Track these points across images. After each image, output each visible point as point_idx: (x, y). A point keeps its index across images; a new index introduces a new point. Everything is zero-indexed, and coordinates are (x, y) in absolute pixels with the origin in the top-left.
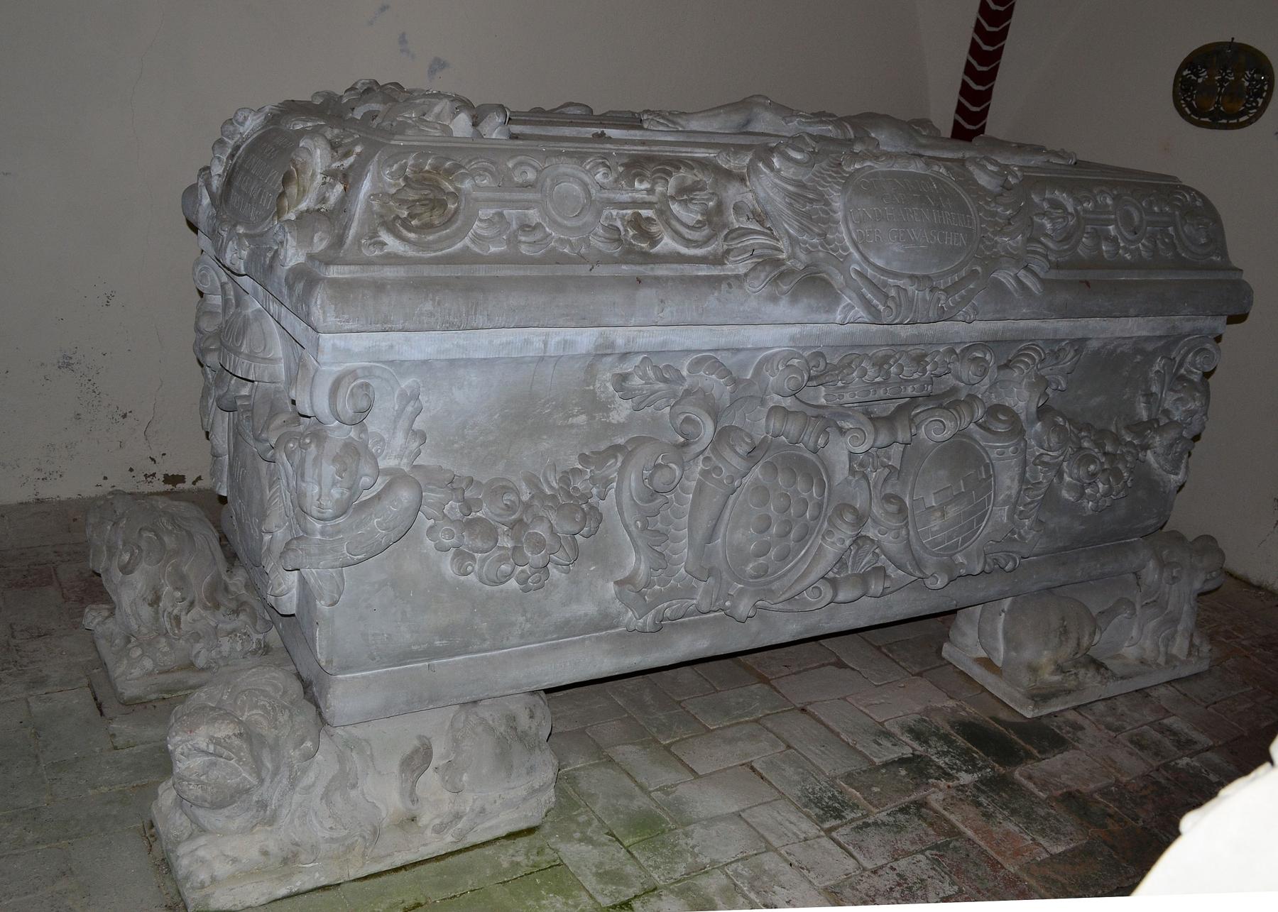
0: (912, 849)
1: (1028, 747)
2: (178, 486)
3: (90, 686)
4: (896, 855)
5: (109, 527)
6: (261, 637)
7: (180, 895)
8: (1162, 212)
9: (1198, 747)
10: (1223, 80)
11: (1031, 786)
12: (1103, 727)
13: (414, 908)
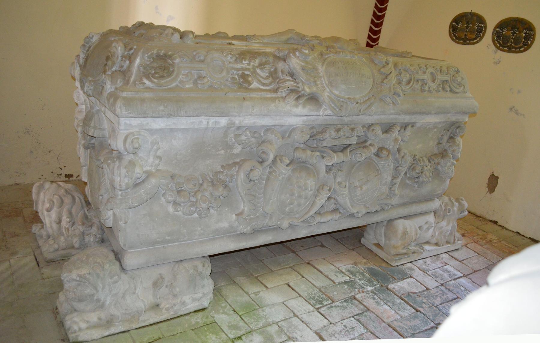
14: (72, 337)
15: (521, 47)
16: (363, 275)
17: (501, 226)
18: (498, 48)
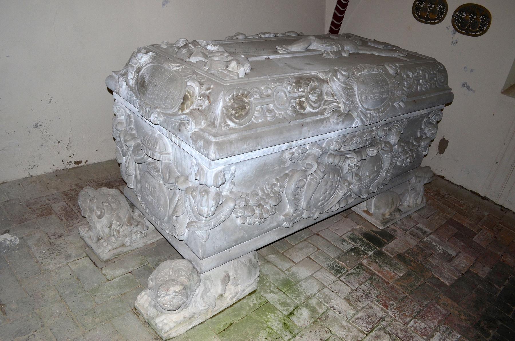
0: (364, 281)
1: (384, 239)
2: (80, 164)
3: (87, 256)
4: (360, 283)
5: (88, 201)
6: (145, 232)
7: (157, 334)
8: (434, 73)
9: (428, 233)
10: (430, 7)
11: (388, 253)
12: (401, 230)
13: (231, 325)
14: (164, 336)
15: (477, 32)
16: (363, 241)
17: (447, 180)
18: (456, 30)
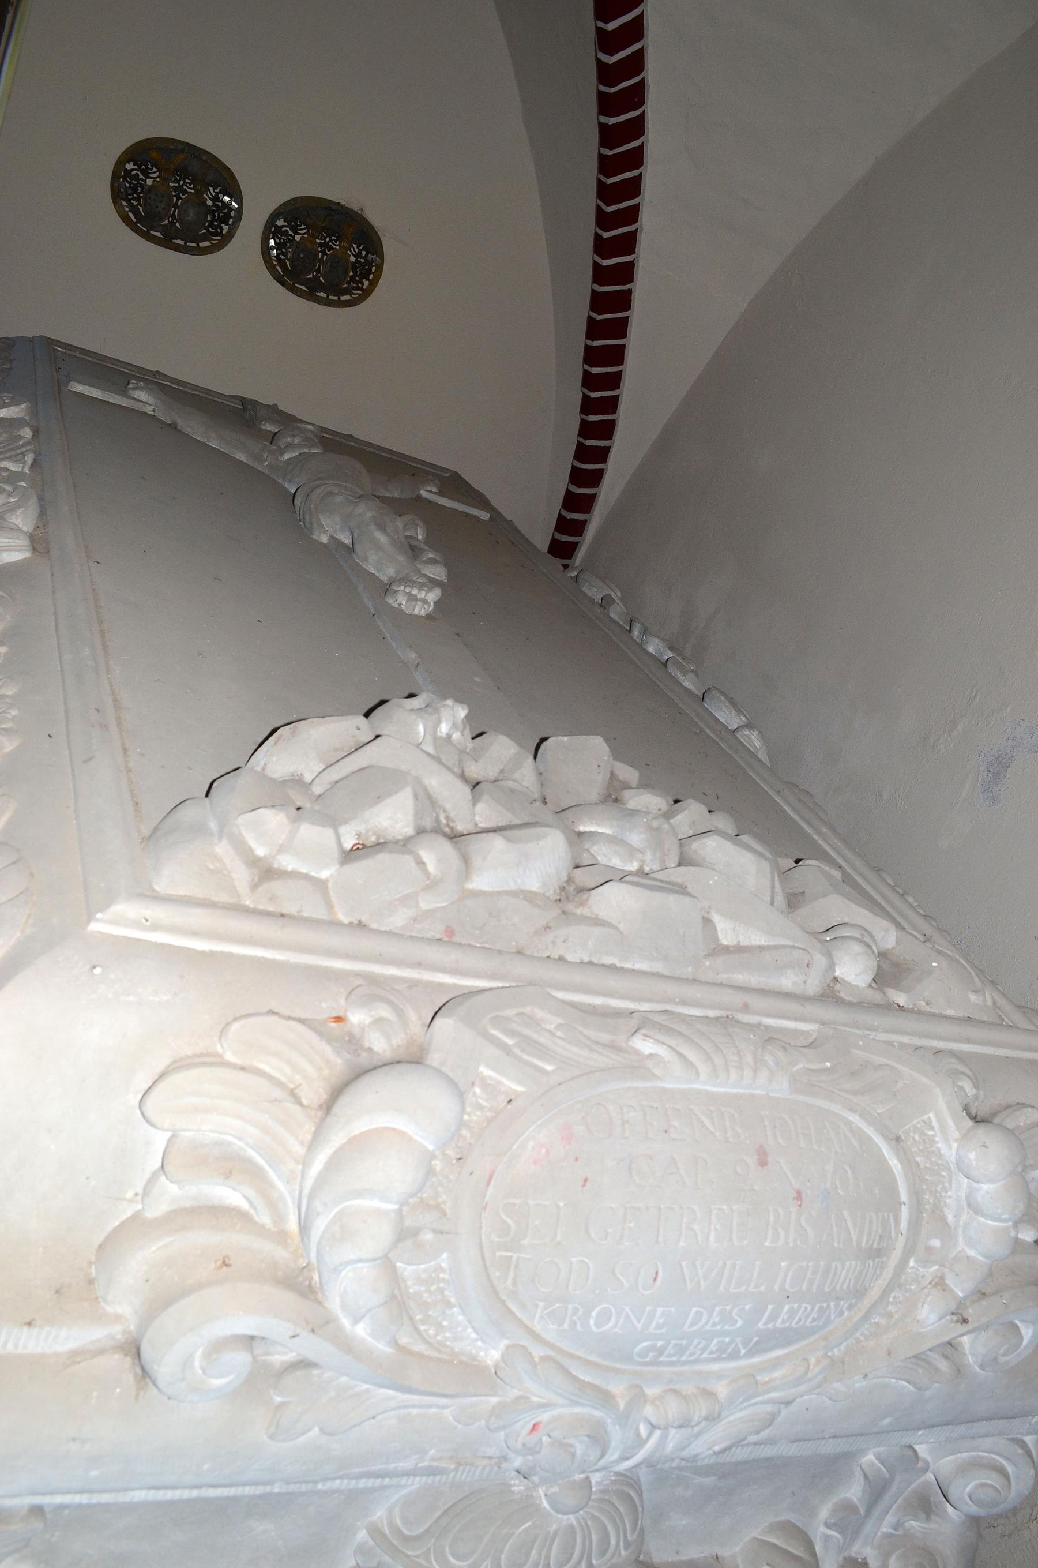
15: (205, 238)
